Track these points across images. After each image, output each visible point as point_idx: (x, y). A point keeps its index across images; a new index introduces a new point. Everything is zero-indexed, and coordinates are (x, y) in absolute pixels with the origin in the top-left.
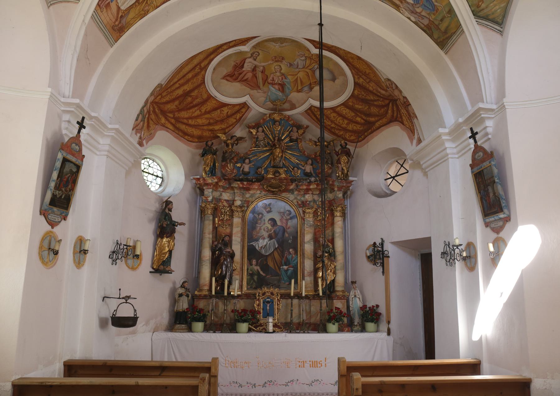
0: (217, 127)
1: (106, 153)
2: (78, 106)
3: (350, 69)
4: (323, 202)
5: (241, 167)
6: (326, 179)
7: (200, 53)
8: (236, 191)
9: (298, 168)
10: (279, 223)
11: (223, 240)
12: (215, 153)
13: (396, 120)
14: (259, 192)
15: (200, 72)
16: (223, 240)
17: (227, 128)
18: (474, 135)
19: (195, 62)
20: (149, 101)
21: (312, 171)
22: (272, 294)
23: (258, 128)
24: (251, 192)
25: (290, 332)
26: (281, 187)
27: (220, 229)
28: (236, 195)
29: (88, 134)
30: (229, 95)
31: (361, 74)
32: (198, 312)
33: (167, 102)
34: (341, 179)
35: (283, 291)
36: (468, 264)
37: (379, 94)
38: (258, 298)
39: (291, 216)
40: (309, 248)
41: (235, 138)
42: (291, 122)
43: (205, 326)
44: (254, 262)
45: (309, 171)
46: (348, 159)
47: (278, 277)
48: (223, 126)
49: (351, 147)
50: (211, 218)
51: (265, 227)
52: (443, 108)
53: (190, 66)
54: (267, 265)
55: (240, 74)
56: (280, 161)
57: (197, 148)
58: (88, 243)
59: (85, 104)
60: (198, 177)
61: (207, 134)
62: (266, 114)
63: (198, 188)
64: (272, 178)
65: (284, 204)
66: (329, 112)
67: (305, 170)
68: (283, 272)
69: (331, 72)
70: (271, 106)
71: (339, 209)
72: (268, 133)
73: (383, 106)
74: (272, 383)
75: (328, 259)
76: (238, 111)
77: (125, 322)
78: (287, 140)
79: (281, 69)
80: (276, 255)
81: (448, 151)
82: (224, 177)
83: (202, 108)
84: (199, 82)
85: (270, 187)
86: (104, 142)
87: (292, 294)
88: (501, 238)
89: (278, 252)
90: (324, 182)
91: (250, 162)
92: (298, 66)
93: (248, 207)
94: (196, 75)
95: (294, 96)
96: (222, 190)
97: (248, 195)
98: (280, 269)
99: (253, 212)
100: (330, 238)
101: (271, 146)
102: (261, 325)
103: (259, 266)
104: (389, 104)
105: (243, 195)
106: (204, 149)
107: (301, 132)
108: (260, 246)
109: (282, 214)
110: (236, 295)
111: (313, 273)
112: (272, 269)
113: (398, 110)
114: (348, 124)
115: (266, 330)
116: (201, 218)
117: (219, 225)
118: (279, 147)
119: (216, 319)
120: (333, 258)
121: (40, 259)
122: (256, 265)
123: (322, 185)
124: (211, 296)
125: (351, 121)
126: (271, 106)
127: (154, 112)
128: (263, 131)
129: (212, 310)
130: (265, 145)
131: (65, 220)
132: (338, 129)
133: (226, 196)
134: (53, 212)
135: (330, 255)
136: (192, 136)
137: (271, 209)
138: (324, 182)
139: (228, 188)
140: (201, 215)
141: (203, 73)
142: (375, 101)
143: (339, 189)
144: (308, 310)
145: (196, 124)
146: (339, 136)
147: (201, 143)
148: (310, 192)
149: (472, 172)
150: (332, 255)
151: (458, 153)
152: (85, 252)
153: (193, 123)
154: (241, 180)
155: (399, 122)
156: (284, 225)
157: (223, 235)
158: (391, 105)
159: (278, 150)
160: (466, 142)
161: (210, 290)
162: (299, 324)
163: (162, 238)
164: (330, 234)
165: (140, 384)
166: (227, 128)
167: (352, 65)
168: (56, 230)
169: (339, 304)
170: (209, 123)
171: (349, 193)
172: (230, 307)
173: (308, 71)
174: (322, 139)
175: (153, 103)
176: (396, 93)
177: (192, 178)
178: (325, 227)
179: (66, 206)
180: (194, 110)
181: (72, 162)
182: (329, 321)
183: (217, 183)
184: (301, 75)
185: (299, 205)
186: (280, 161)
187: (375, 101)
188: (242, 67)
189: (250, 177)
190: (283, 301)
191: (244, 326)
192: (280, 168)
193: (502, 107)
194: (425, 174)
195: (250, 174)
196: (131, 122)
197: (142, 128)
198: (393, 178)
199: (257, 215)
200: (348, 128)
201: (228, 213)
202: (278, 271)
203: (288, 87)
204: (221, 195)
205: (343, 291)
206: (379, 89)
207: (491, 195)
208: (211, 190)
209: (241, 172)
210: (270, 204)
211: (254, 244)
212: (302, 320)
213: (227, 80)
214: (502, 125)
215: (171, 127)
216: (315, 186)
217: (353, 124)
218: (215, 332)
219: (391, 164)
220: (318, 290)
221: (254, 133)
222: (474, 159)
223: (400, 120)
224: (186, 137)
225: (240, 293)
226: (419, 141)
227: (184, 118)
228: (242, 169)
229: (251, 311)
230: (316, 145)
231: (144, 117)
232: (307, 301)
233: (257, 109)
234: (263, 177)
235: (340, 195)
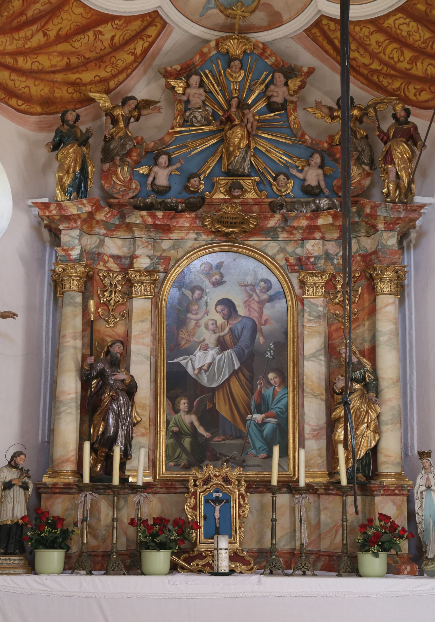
0: (87, 76)
4: (347, 260)
5: (148, 175)
6: (355, 203)
8: (137, 233)
9: (288, 177)
10: (241, 311)
12: (83, 141)
14: (192, 235)
16: (108, 353)
17: (114, 76)
21: (323, 184)
22: (227, 480)
23: (188, 78)
24: (175, 236)
25: (271, 573)
26: (245, 222)
27: (101, 327)
28: (138, 242)
32: (49, 525)
34: (393, 202)
35: (252, 474)
38: (192, 490)
39: (271, 292)
40: (314, 370)
41: (132, 104)
42: (270, 61)
43: (67, 557)
44: (183, 404)
45: (314, 183)
46: (413, 151)
47: (240, 441)
48: (103, 74)
50: (79, 299)
51: (207, 323)
56: (244, 159)
57: (41, 128)
60: (46, 200)
61: (63, 93)
62: (207, 41)
63: (46, 226)
64: (225, 201)
65: (256, 263)
66: (366, 31)
67: (304, 180)
68: (253, 429)
70: (221, 19)
71: (389, 274)
72: (215, 88)
75: (362, 396)
76: (139, 35)
78: (261, 105)
80: (235, 386)
82: (108, 200)
83: (50, 26)
85: (220, 222)
87: (275, 482)
89: (240, 381)
90: (350, 209)
91: (170, 163)
93: (166, 272)
96: (103, 231)
97: (166, 244)
98: (244, 421)
99: (180, 284)
100: (367, 346)
101: (222, 123)
102: (200, 556)
103: (196, 414)
106: (58, 132)
107: (294, 84)
108: (197, 366)
109: (249, 288)
110: (140, 483)
111: (324, 432)
112: (222, 425)
114: (413, 61)
115: (212, 568)
116: (56, 299)
117: (98, 317)
118: (240, 125)
119: (94, 543)
120: (372, 395)
122: (189, 412)
123: (344, 216)
124: (81, 488)
126: (221, 19)
128: (202, 84)
129: (84, 520)
130: (206, 119)
132: (387, 75)
133: (114, 246)
135: (366, 386)
136: (28, 99)
137: (225, 278)
138: (350, 209)
139: (118, 227)
143: (390, 226)
144: (314, 522)
145: (35, 67)
146: (391, 94)
147: (51, 117)
148: (318, 235)
150: (371, 388)
153: (28, 66)
154: (150, 208)
156: (255, 315)
157: (109, 340)
159: (239, 132)
161: (79, 472)
162: (292, 553)
164: (367, 336)
166: (114, 76)
169: (388, 507)
170: (68, 64)
171: (413, 235)
172: (127, 514)
174: (346, 101)
177: (30, 202)
178: (351, 319)
180: (27, 31)
182: (366, 545)
183: (91, 215)
185: (291, 265)
186: (244, 159)
189: (170, 199)
190: (254, 499)
191: (160, 559)
192: (243, 175)
195: (171, 193)
199: (188, 293)
200: (413, 72)
201: (119, 288)
202: (241, 426)
204: (102, 243)
205: (398, 476)
208: (76, 233)
209: (149, 188)
210: (219, 266)
211: (181, 360)
212: (298, 544)
216: (330, 220)
217: (428, 61)
218: (90, 573)
220: (338, 473)
221: (180, 90)
224: (13, 102)
225: (149, 479)
228: (150, 179)
229: (176, 522)
230: (333, 118)
232: (312, 498)
234: (203, 199)
235: (391, 240)
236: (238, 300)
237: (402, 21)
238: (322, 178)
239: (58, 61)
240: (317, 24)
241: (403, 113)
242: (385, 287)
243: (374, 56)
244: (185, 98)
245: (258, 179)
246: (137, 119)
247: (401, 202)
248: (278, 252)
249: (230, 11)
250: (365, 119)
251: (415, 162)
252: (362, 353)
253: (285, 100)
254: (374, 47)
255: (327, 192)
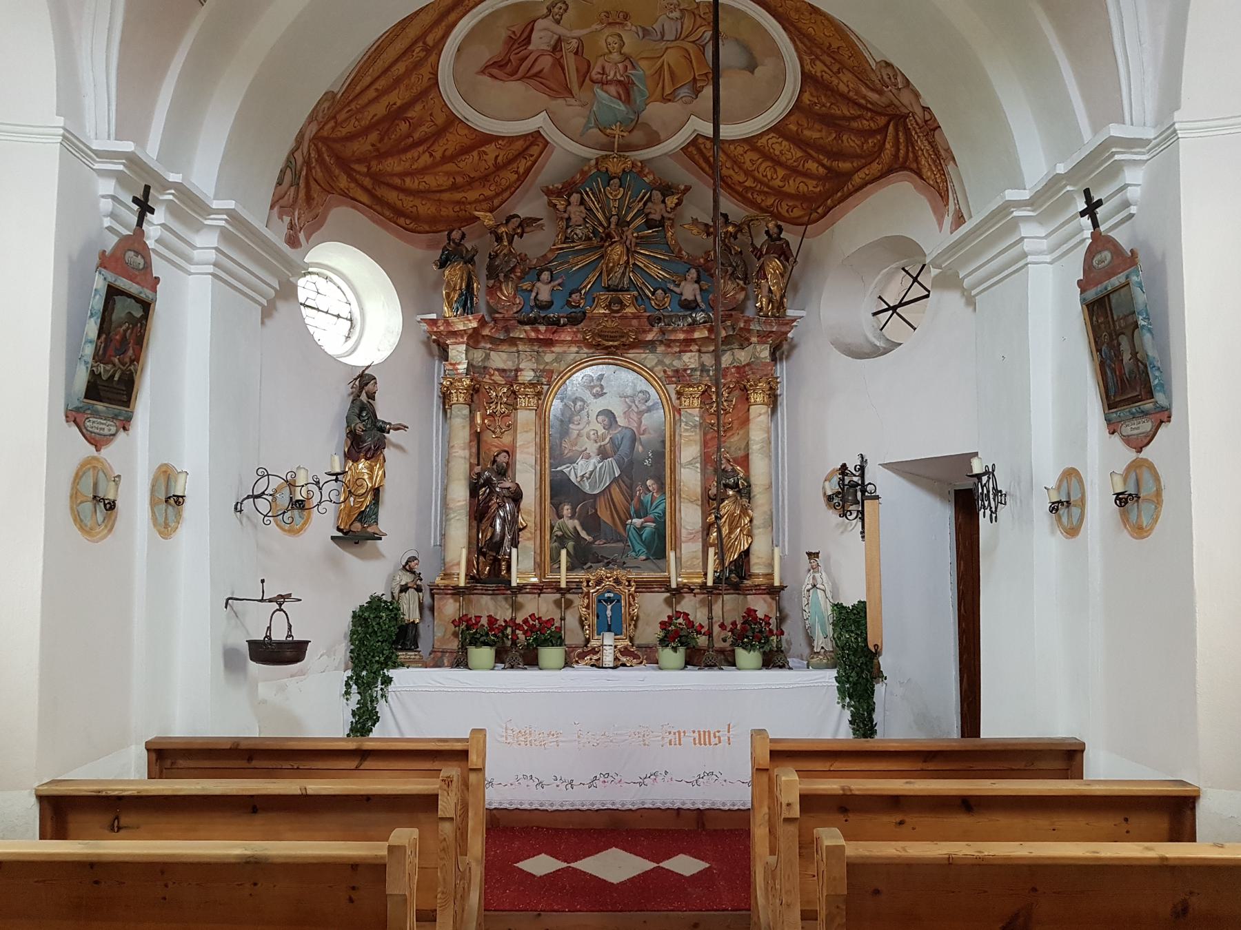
0: (472, 195)
1: (211, 269)
2: (132, 161)
3: (792, 39)
5: (531, 291)
7: (422, 9)
10: (621, 421)
11: (494, 461)
13: (904, 167)
14: (574, 349)
15: (425, 58)
16: (494, 461)
18: (1091, 209)
19: (412, 32)
20: (307, 138)
21: (699, 298)
22: (617, 581)
23: (569, 196)
24: (557, 349)
28: (523, 356)
29: (163, 225)
30: (500, 113)
31: (819, 52)
33: (351, 137)
34: (766, 316)
36: (1065, 519)
37: (863, 102)
39: (650, 403)
40: (690, 478)
41: (515, 222)
45: (691, 298)
47: (621, 545)
48: (488, 193)
49: (790, 236)
52: (1020, 145)
53: (400, 46)
54: (595, 516)
55: (523, 59)
57: (430, 246)
58: (181, 478)
59: (151, 152)
60: (434, 316)
61: (447, 212)
66: (740, 150)
68: (633, 533)
69: (746, 48)
73: (872, 133)
74: (610, 779)
76: (521, 154)
77: (280, 653)
78: (640, 221)
79: (622, 46)
80: (616, 492)
81: (1027, 246)
83: (436, 147)
84: (425, 83)
85: (600, 336)
86: (205, 244)
87: (563, 585)
88: (1146, 460)
92: (663, 36)
94: (417, 65)
95: (656, 112)
96: (489, 346)
97: (548, 358)
98: (624, 525)
104: (887, 125)
105: (538, 357)
106: (444, 249)
107: (671, 201)
112: (609, 527)
113: (910, 142)
114: (784, 179)
116: (445, 411)
121: (75, 521)
122: (571, 518)
125: (794, 171)
127: (321, 161)
128: (582, 202)
131: (125, 429)
132: (760, 192)
133: (500, 359)
134: (96, 414)
136: (416, 218)
140: (444, 405)
141: (432, 58)
142: (854, 118)
143: (763, 336)
149: (1083, 301)
150: (744, 491)
151: (1052, 251)
152: (179, 500)
154: (532, 322)
155: (912, 170)
156: (634, 426)
158: (891, 128)
159: (618, 249)
160: (1074, 224)
163: (356, 460)
165: (310, 792)
166: (498, 195)
167: (798, 30)
168: (105, 453)
170: (454, 184)
171: (785, 347)
173: (689, 46)
175: (316, 139)
176: (906, 97)
177: (419, 318)
179: (125, 398)
180: (414, 153)
181: (130, 296)
184: (672, 57)
185: (669, 377)
186: (624, 273)
187: (854, 118)
188: (528, 40)
193: (1170, 135)
194: (971, 302)
196: (267, 191)
197: (295, 201)
198: (894, 309)
203: (640, 90)
204: (487, 357)
206: (864, 90)
207: (1127, 357)
209: (532, 303)
210: (601, 377)
211: (565, 468)
213: (492, 76)
214: (1166, 186)
215: (364, 198)
216: (706, 334)
217: (799, 179)
219: (889, 277)
222: (1088, 267)
223: (914, 166)
224: (402, 221)
226: (959, 220)
227: (392, 175)
228: (534, 294)
230: (708, 235)
231: (296, 176)
233: (567, 150)
235: (765, 353)
236: (618, 411)
237: (774, 140)
238: (698, 292)
239: (445, 182)
240: (694, 142)
241: (776, 230)
242: (757, 397)
243: (748, 173)
244: (566, 215)
245: (635, 293)
246: (521, 237)
247: (773, 316)
248: (656, 365)
249: (608, 131)
250: (739, 235)
251: (787, 275)
252: (736, 461)
253: (663, 217)
254: (748, 165)
255: (703, 306)
